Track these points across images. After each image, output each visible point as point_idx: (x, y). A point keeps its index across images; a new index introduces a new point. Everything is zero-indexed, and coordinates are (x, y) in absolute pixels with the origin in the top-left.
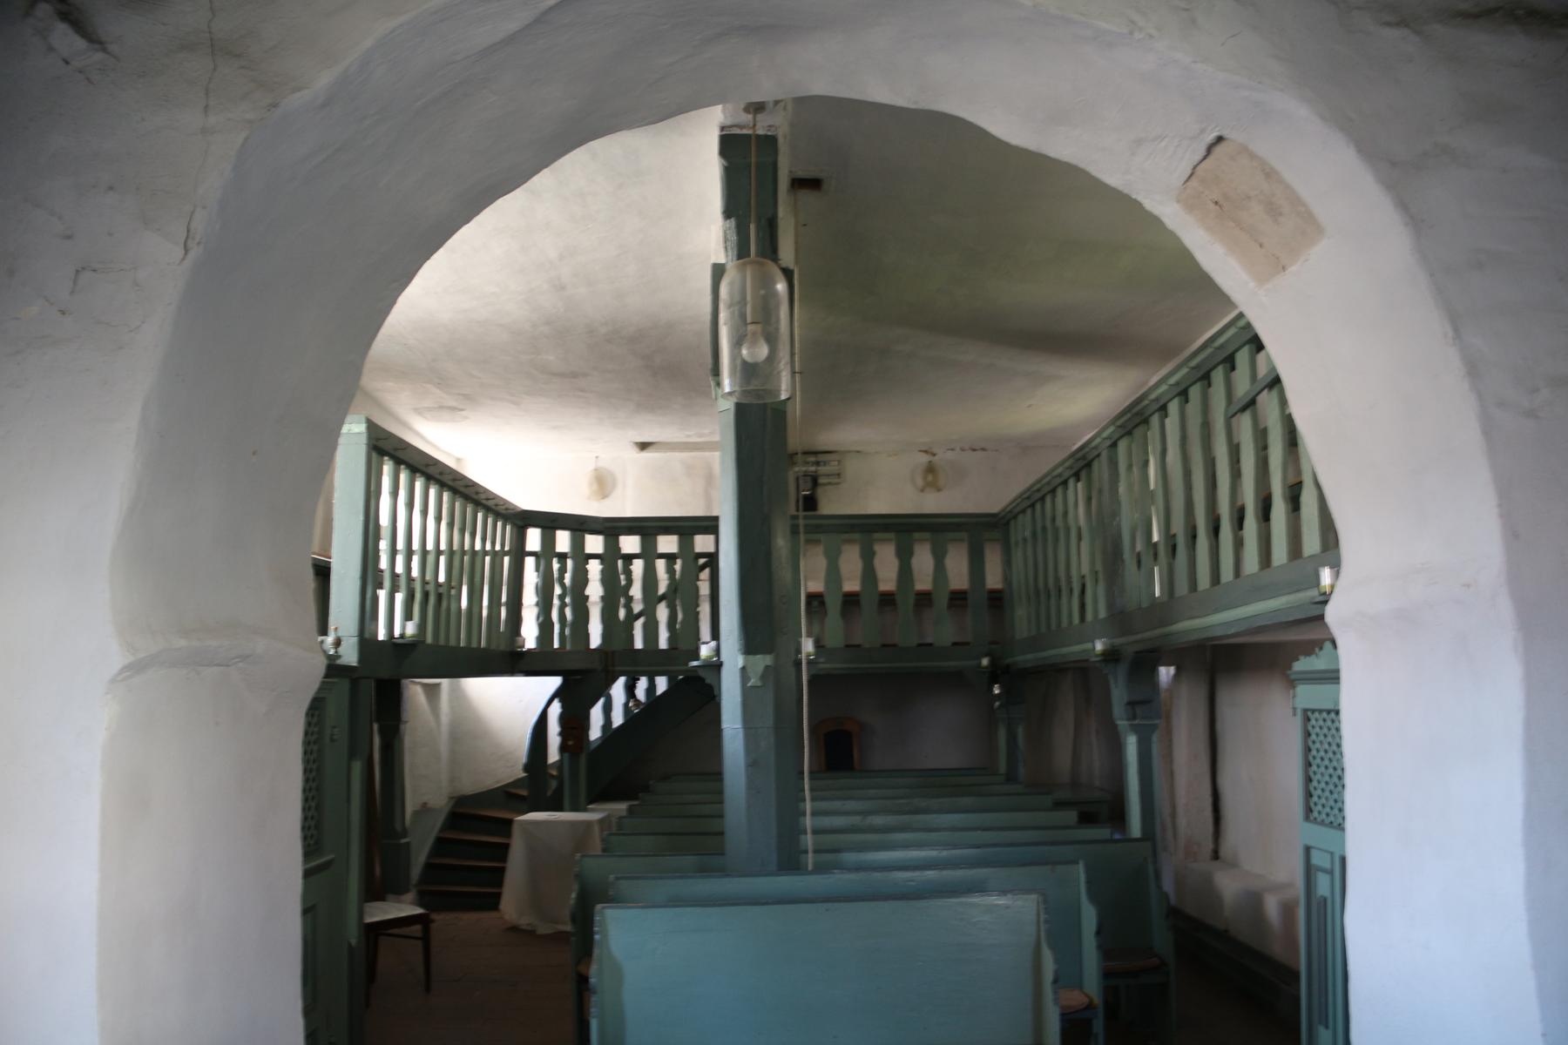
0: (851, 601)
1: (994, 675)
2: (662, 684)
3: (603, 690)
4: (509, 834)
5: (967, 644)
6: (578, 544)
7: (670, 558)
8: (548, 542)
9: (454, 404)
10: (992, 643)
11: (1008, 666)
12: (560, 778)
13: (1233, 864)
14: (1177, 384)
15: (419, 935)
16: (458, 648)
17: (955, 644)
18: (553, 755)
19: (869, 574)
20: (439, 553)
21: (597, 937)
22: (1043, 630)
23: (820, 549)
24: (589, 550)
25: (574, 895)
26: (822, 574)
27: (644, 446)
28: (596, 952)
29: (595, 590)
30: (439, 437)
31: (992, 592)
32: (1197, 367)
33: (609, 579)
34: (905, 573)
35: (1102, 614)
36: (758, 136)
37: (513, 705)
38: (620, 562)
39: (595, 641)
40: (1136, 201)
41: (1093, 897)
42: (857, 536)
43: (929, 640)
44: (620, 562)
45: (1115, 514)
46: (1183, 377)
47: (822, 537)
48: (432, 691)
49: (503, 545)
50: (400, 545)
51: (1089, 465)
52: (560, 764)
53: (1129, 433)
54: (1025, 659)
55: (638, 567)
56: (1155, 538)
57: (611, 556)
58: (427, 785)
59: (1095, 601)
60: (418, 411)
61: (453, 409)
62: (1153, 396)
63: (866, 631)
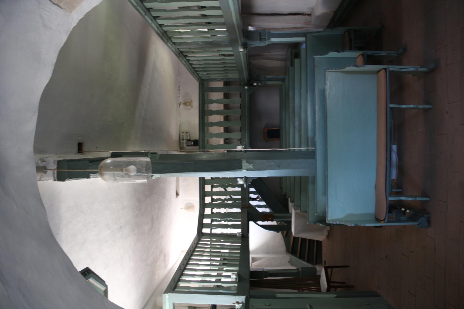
0: (227, 130)
1: (250, 85)
2: (252, 189)
3: (253, 208)
4: (298, 238)
5: (240, 93)
6: (208, 216)
7: (213, 187)
8: (207, 226)
9: (163, 257)
10: (240, 85)
11: (248, 80)
12: (281, 221)
13: (313, 9)
14: (151, 20)
15: (331, 269)
16: (240, 257)
17: (240, 97)
18: (274, 223)
19: (218, 124)
20: (210, 260)
21: (338, 223)
22: (236, 68)
23: (210, 140)
24: (210, 213)
25: (321, 225)
26: (218, 139)
27: (177, 194)
28: (343, 223)
29: (223, 211)
30: (174, 260)
31: (224, 85)
32: (145, 12)
33: (219, 206)
34: (217, 113)
35: (231, 49)
36: (58, 168)
37: (258, 235)
38: (214, 203)
39: (239, 210)
40: (73, 29)
41: (326, 53)
42: (206, 128)
43: (239, 105)
44: (214, 203)
45: (197, 43)
46: (149, 18)
47: (206, 139)
48: (254, 260)
49: (208, 241)
50: (208, 268)
51: (182, 52)
52: (277, 222)
53: (170, 38)
54: (245, 75)
55: (215, 197)
56: (206, 30)
57: (211, 206)
58: (282, 262)
59: (227, 51)
60: (166, 267)
61: (165, 256)
62: (157, 29)
63: (236, 125)
